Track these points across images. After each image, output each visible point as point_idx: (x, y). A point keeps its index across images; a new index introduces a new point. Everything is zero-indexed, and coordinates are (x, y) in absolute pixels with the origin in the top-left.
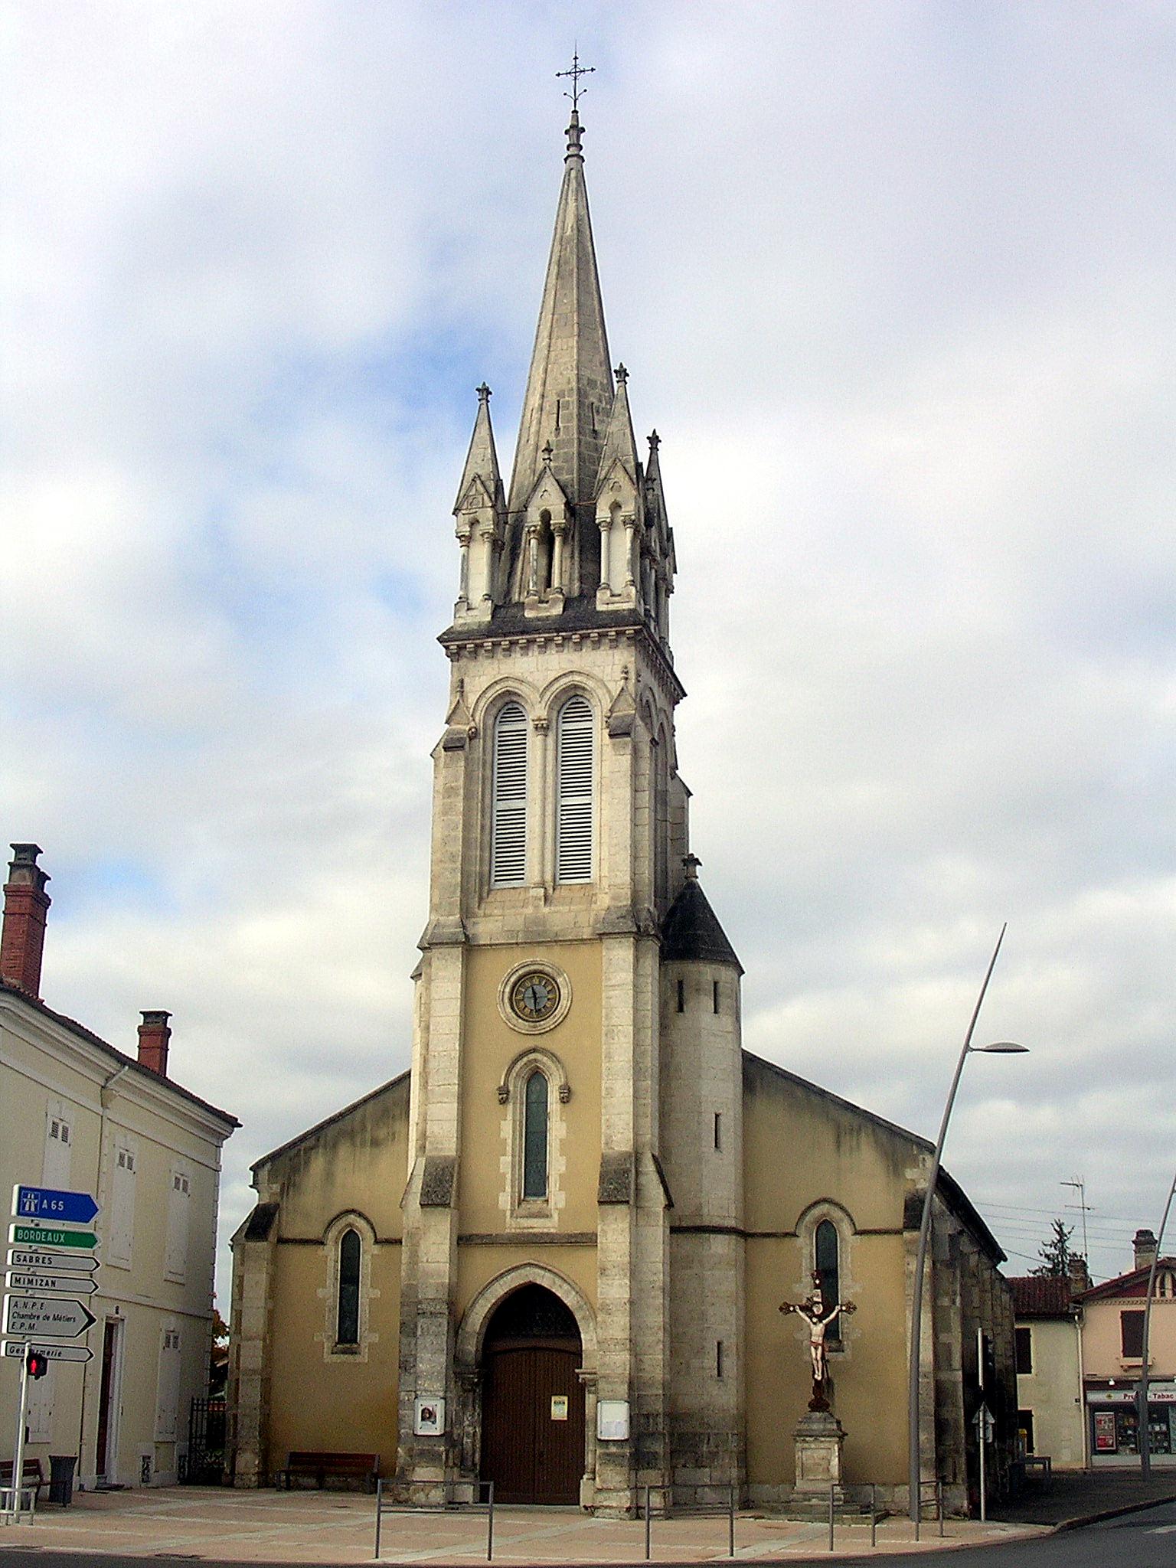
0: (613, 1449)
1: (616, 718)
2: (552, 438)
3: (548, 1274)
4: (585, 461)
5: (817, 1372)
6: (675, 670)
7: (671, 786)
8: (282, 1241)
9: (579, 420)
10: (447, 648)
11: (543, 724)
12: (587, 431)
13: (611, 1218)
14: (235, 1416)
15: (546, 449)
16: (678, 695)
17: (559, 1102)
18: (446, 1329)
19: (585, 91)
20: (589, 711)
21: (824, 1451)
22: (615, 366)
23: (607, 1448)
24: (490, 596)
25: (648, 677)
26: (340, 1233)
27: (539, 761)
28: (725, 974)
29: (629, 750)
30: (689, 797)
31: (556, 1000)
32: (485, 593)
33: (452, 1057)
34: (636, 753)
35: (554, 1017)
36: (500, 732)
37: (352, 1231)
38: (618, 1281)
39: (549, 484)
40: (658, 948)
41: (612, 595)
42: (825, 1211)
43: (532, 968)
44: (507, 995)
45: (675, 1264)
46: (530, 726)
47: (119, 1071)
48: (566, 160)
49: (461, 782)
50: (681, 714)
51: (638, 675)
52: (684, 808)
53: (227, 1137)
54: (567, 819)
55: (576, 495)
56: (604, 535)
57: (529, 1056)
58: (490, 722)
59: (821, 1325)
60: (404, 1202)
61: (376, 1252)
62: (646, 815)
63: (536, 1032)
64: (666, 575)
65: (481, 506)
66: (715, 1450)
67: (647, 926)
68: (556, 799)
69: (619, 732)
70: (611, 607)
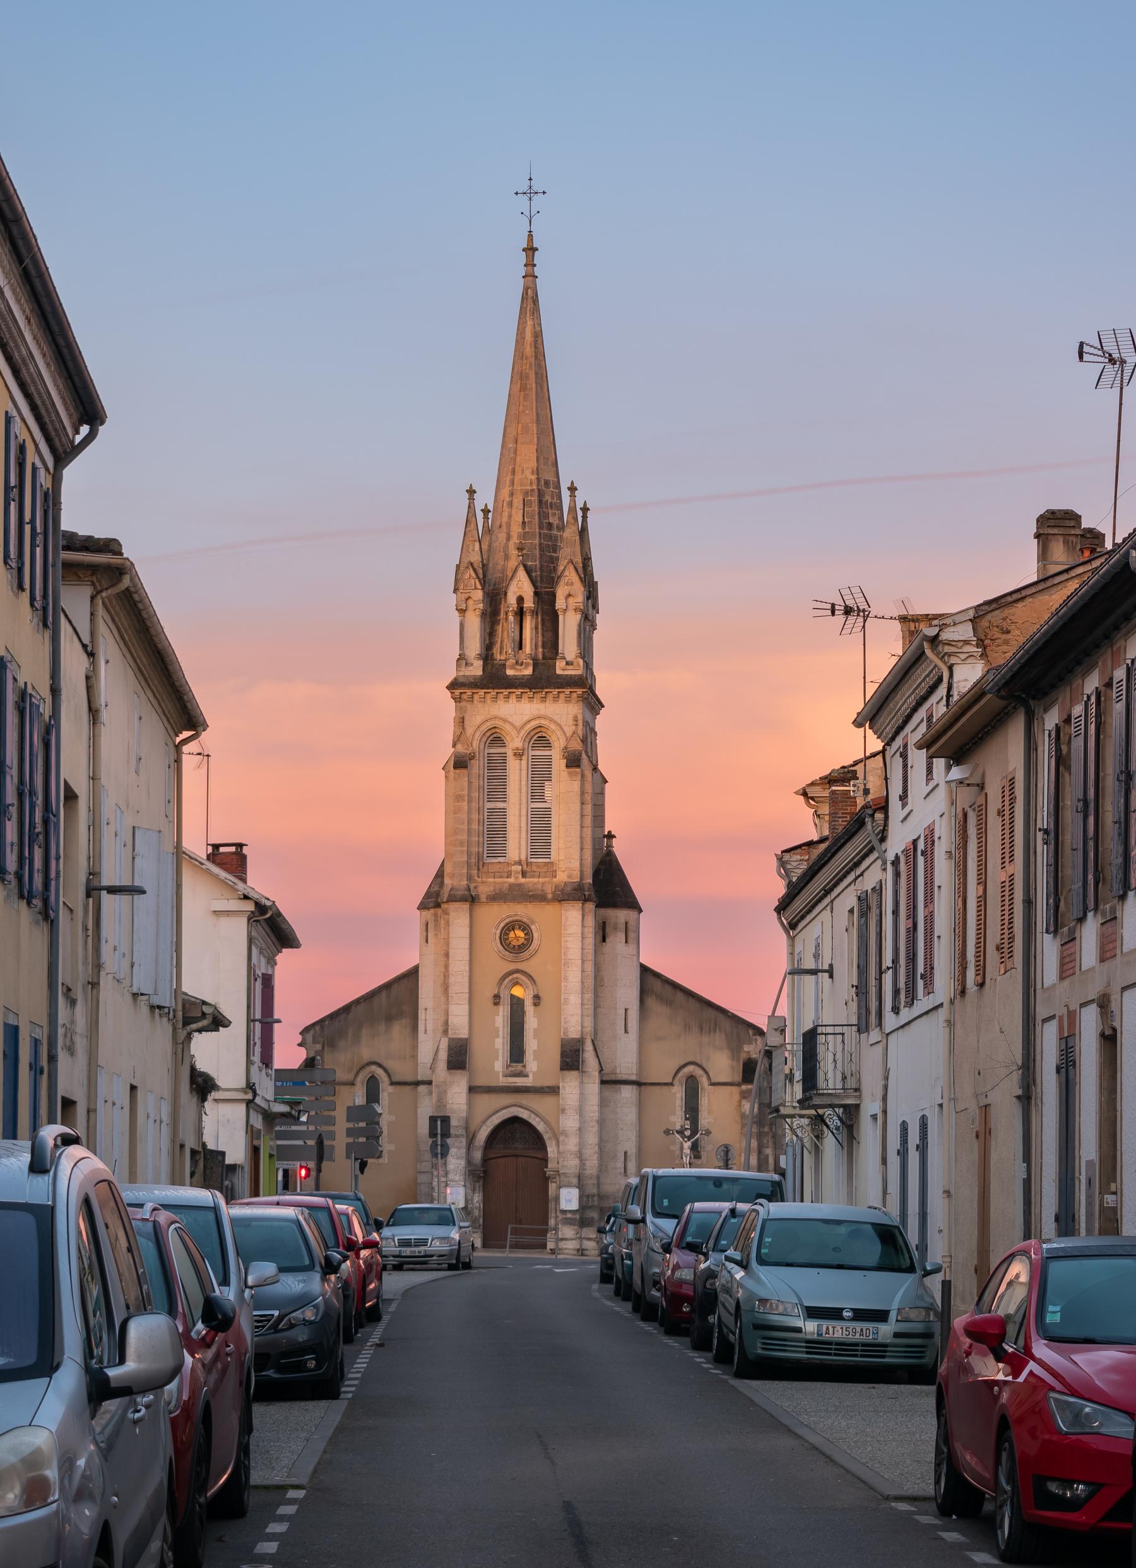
0: (569, 1215)
3: (526, 1111)
9: (540, 516)
19: (538, 212)
27: (517, 778)
29: (579, 777)
34: (583, 776)
37: (373, 1077)
39: (522, 574)
41: (568, 663)
43: (515, 918)
45: (603, 1103)
49: (466, 792)
55: (539, 579)
56: (561, 618)
58: (482, 747)
61: (391, 1091)
67: (590, 895)
70: (566, 673)
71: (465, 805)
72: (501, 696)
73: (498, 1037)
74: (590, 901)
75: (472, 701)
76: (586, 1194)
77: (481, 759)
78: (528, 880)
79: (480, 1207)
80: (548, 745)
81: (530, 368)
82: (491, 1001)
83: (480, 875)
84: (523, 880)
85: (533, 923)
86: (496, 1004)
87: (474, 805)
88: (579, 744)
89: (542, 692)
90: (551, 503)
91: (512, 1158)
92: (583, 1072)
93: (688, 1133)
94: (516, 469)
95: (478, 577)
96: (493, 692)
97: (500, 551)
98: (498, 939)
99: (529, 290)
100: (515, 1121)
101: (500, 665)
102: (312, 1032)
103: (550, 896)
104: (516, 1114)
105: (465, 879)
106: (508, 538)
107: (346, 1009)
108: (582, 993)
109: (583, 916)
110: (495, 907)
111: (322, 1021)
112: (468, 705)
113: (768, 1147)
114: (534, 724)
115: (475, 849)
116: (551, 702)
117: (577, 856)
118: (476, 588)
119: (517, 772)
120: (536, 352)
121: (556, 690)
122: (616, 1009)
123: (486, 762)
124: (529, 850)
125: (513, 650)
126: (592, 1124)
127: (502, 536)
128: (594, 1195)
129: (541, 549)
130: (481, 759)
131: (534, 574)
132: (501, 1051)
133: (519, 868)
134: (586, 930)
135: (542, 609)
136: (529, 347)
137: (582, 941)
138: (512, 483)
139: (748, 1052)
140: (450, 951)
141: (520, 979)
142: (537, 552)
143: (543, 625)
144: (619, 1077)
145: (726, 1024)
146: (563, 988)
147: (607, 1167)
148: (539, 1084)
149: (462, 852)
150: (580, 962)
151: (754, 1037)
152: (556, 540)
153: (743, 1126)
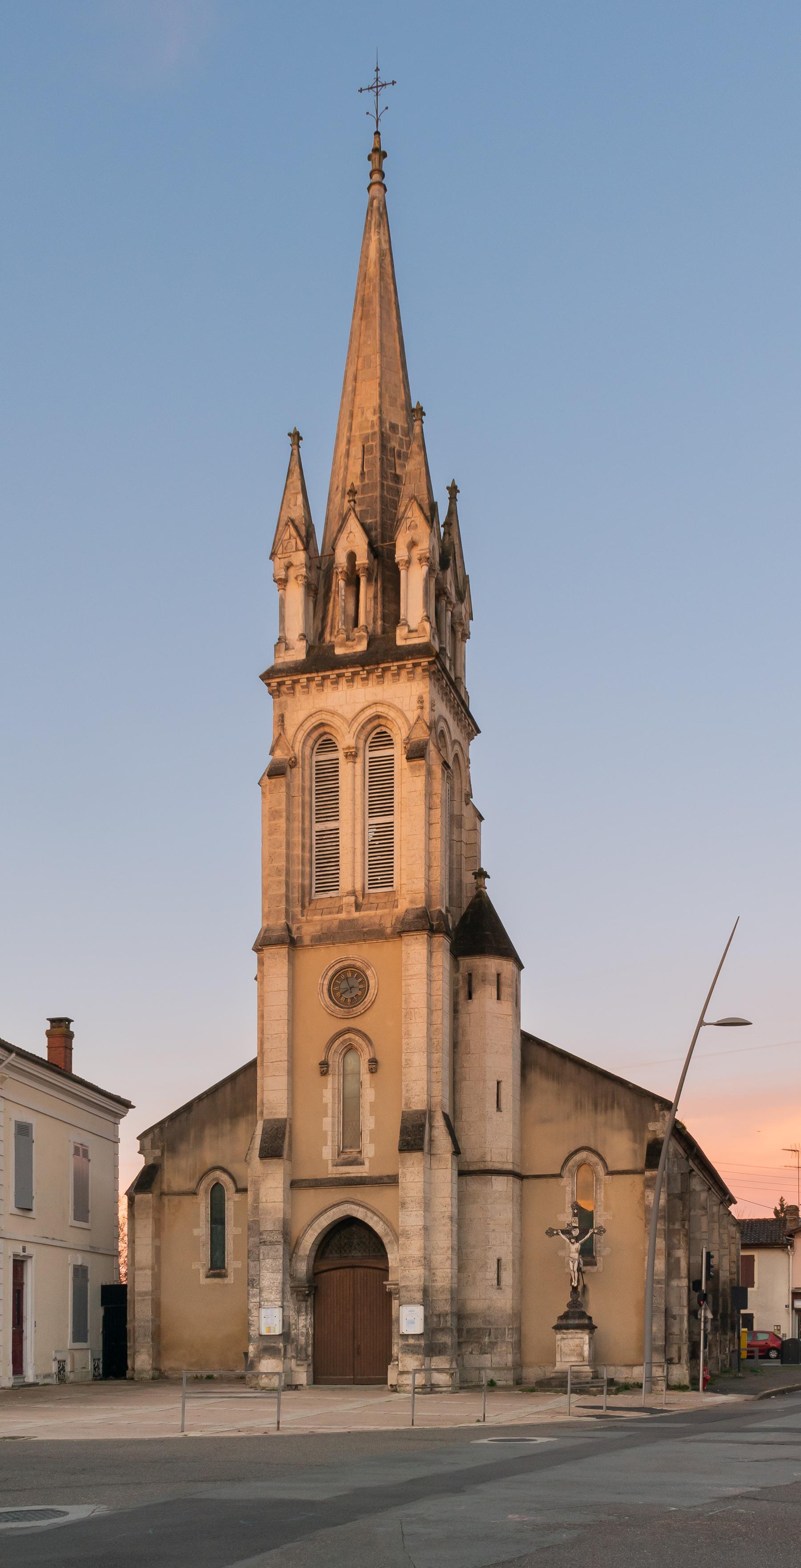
0: (411, 1341)
2: (357, 483)
3: (361, 1209)
5: (574, 1280)
6: (470, 710)
7: (467, 812)
8: (162, 1194)
10: (268, 685)
11: (351, 752)
12: (389, 475)
13: (409, 1163)
14: (134, 1328)
15: (350, 491)
16: (472, 731)
17: (368, 1071)
18: (282, 1253)
20: (391, 740)
21: (578, 1340)
23: (407, 1340)
24: (305, 636)
25: (443, 709)
26: (209, 1185)
28: (507, 966)
29: (423, 772)
30: (481, 821)
31: (365, 989)
33: (283, 1038)
34: (429, 773)
36: (316, 762)
37: (217, 1184)
38: (416, 1213)
39: (353, 525)
41: (410, 631)
42: (584, 1157)
43: (346, 963)
45: (462, 1199)
46: (340, 755)
47: (7, 1058)
48: (369, 189)
50: (476, 748)
51: (433, 705)
52: (476, 830)
53: (124, 1116)
54: (379, 844)
55: (379, 537)
56: (403, 573)
57: (345, 1036)
58: (308, 751)
59: (578, 1244)
60: (248, 1157)
61: (237, 1199)
63: (350, 1016)
64: (462, 619)
65: (294, 549)
66: (495, 1340)
69: (416, 753)
71: (282, 823)
73: (326, 1116)
74: (440, 932)
75: (294, 694)
76: (436, 1312)
77: (307, 768)
78: (362, 913)
79: (307, 1334)
80: (390, 743)
81: (374, 290)
82: (317, 1069)
83: (305, 913)
84: (356, 915)
85: (368, 967)
86: (324, 1073)
87: (297, 825)
88: (425, 732)
89: (377, 669)
91: (348, 1270)
92: (431, 1155)
93: (576, 1233)
94: (356, 411)
95: (299, 535)
97: (335, 517)
100: (348, 1223)
101: (329, 647)
102: (150, 1136)
103: (389, 931)
104: (349, 1213)
105: (283, 916)
107: (188, 1108)
108: (429, 1053)
109: (430, 953)
110: (323, 951)
111: (162, 1123)
113: (679, 1248)
114: (369, 713)
115: (297, 881)
116: (390, 682)
118: (297, 550)
119: (350, 778)
120: (380, 273)
121: (395, 664)
122: (485, 1081)
123: (314, 772)
125: (345, 623)
126: (443, 1222)
128: (447, 1314)
129: (382, 503)
130: (307, 768)
131: (373, 533)
132: (330, 1133)
133: (353, 899)
135: (383, 574)
138: (350, 429)
139: (655, 1131)
142: (378, 507)
144: (490, 1166)
145: (627, 1098)
146: (404, 1047)
147: (474, 1278)
148: (376, 1173)
149: (280, 882)
150: (425, 1011)
151: (661, 1113)
153: (647, 1222)
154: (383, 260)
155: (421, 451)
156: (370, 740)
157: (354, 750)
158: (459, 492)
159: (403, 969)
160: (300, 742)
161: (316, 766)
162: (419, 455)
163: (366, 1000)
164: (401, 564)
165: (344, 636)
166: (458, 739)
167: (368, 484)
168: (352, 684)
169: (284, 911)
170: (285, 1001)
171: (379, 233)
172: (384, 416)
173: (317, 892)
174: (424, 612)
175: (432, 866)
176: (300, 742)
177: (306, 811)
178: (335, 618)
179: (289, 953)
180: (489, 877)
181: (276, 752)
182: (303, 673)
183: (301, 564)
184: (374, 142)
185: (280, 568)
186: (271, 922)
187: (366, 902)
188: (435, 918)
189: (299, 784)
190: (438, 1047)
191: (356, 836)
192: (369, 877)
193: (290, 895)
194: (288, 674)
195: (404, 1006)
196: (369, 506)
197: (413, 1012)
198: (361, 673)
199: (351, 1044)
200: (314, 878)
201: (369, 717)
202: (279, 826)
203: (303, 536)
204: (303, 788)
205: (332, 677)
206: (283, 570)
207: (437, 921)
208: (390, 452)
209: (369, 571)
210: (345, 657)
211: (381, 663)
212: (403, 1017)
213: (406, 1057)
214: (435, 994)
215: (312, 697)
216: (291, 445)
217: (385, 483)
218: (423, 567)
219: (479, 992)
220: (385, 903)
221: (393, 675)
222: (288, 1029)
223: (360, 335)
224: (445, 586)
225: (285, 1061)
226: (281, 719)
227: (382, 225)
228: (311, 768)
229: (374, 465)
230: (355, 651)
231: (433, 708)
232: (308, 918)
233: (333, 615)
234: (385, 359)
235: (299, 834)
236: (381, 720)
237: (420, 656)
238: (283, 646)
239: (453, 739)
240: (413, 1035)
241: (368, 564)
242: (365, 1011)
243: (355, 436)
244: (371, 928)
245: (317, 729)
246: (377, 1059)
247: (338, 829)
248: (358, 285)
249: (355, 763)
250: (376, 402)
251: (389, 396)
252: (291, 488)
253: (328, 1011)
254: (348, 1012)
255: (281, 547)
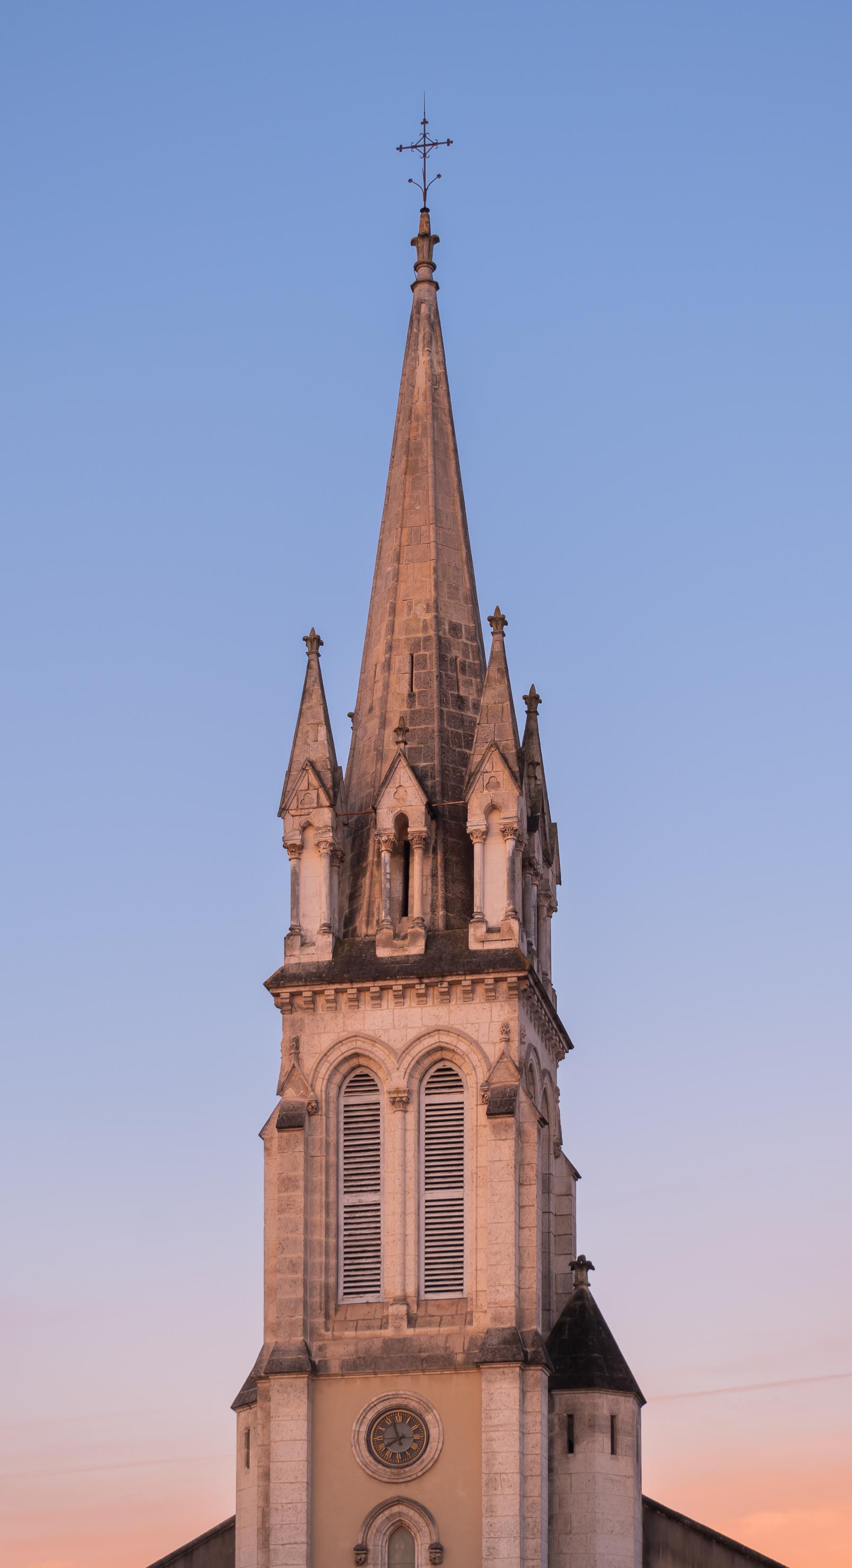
1: (493, 1090)
4: (448, 741)
7: (556, 1168)
9: (440, 683)
10: (276, 995)
19: (439, 176)
20: (460, 1080)
22: (486, 611)
24: (330, 927)
25: (533, 1037)
27: (398, 1145)
28: (624, 1404)
29: (512, 1134)
30: (576, 1180)
31: (424, 1441)
32: (323, 922)
33: (299, 1510)
34: (520, 1133)
35: (421, 1463)
36: (345, 1106)
39: (404, 776)
40: (547, 1378)
41: (490, 930)
43: (394, 1402)
44: (363, 1436)
48: (413, 287)
49: (300, 1172)
51: (522, 1035)
55: (438, 789)
56: (477, 849)
57: (392, 1508)
58: (333, 1093)
62: (532, 1216)
65: (315, 805)
68: (419, 1193)
70: (488, 946)
71: (298, 1195)
72: (366, 996)
74: (537, 1363)
75: (314, 1009)
77: (332, 1115)
78: (418, 1330)
80: (457, 1085)
81: (424, 434)
83: (330, 1326)
84: (409, 1332)
85: (429, 1409)
87: (319, 1198)
88: (512, 1075)
89: (442, 982)
90: (463, 664)
95: (323, 785)
96: (352, 989)
97: (369, 752)
98: (363, 1442)
99: (423, 306)
103: (460, 1358)
105: (300, 1332)
106: (383, 724)
108: (523, 1539)
109: (523, 1393)
110: (359, 1382)
112: (307, 1018)
114: (428, 1043)
115: (319, 1279)
116: (460, 1002)
117: (509, 1280)
118: (319, 806)
119: (398, 1134)
120: (433, 408)
121: (468, 977)
124: (423, 1278)
125: (390, 912)
127: (375, 723)
129: (442, 739)
130: (332, 1115)
131: (429, 783)
133: (403, 1309)
134: (529, 1419)
135: (444, 842)
136: (421, 398)
137: (522, 1440)
138: (392, 629)
140: (273, 1467)
141: (406, 1515)
143: (446, 868)
146: (485, 1529)
150: (517, 1478)
152: (472, 729)
154: (435, 389)
155: (503, 678)
156: (427, 1078)
157: (406, 1095)
158: (541, 702)
159: (483, 1415)
160: (323, 1079)
161: (345, 1111)
162: (501, 683)
163: (424, 1456)
164: (475, 836)
165: (391, 932)
166: (549, 1069)
167: (420, 711)
168: (402, 1000)
169: (301, 1323)
170: (304, 1456)
171: (430, 352)
172: (442, 614)
173: (345, 1294)
174: (509, 905)
175: (523, 1268)
176: (323, 1079)
177: (332, 1178)
178: (374, 901)
179: (308, 1385)
180: (593, 1268)
181: (286, 1092)
182: (330, 982)
183: (326, 826)
184: (421, 222)
185: (295, 830)
186: (281, 1339)
187: (423, 1314)
188: (529, 1342)
189: (321, 1139)
190: (535, 1530)
191: (407, 1217)
192: (426, 1275)
193: (308, 1299)
194: (308, 983)
195: (484, 1470)
196: (421, 743)
197: (498, 1479)
198: (417, 987)
199: (400, 1520)
200: (342, 1273)
201: (428, 1049)
202: (294, 1201)
203: (328, 786)
204: (328, 1144)
205: (373, 990)
206: (298, 832)
207: (533, 1347)
208: (451, 665)
209: (425, 841)
210: (392, 963)
211: (447, 976)
212: (483, 1485)
213: (488, 1545)
214: (531, 1453)
215: (341, 1016)
216: (308, 654)
217: (445, 709)
218: (508, 841)
219: (585, 1443)
220: (452, 1316)
221: (465, 992)
222: (307, 1496)
223: (404, 496)
224: (531, 855)
225: (302, 1543)
226: (295, 1044)
227: (433, 339)
228: (338, 1115)
229: (427, 684)
230: (407, 953)
231: (523, 1040)
232: (335, 1333)
233: (370, 897)
234: (441, 531)
235: (321, 1211)
236: (444, 1052)
237: (507, 969)
238: (297, 940)
239: (542, 1068)
240: (499, 1513)
241: (427, 832)
242: (424, 1474)
243: (399, 640)
244: (431, 1353)
245: (347, 1061)
246: (442, 1543)
247: (379, 1204)
248: (398, 420)
249: (405, 1112)
250: (429, 594)
251: (448, 585)
252: (309, 715)
253: (367, 1471)
254: (398, 1475)
255: (295, 800)
